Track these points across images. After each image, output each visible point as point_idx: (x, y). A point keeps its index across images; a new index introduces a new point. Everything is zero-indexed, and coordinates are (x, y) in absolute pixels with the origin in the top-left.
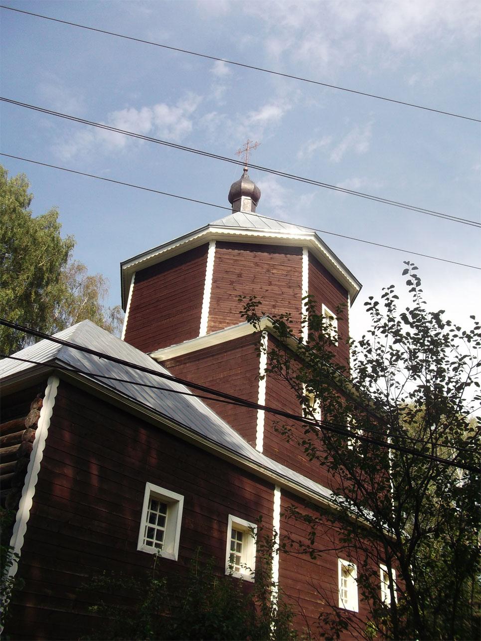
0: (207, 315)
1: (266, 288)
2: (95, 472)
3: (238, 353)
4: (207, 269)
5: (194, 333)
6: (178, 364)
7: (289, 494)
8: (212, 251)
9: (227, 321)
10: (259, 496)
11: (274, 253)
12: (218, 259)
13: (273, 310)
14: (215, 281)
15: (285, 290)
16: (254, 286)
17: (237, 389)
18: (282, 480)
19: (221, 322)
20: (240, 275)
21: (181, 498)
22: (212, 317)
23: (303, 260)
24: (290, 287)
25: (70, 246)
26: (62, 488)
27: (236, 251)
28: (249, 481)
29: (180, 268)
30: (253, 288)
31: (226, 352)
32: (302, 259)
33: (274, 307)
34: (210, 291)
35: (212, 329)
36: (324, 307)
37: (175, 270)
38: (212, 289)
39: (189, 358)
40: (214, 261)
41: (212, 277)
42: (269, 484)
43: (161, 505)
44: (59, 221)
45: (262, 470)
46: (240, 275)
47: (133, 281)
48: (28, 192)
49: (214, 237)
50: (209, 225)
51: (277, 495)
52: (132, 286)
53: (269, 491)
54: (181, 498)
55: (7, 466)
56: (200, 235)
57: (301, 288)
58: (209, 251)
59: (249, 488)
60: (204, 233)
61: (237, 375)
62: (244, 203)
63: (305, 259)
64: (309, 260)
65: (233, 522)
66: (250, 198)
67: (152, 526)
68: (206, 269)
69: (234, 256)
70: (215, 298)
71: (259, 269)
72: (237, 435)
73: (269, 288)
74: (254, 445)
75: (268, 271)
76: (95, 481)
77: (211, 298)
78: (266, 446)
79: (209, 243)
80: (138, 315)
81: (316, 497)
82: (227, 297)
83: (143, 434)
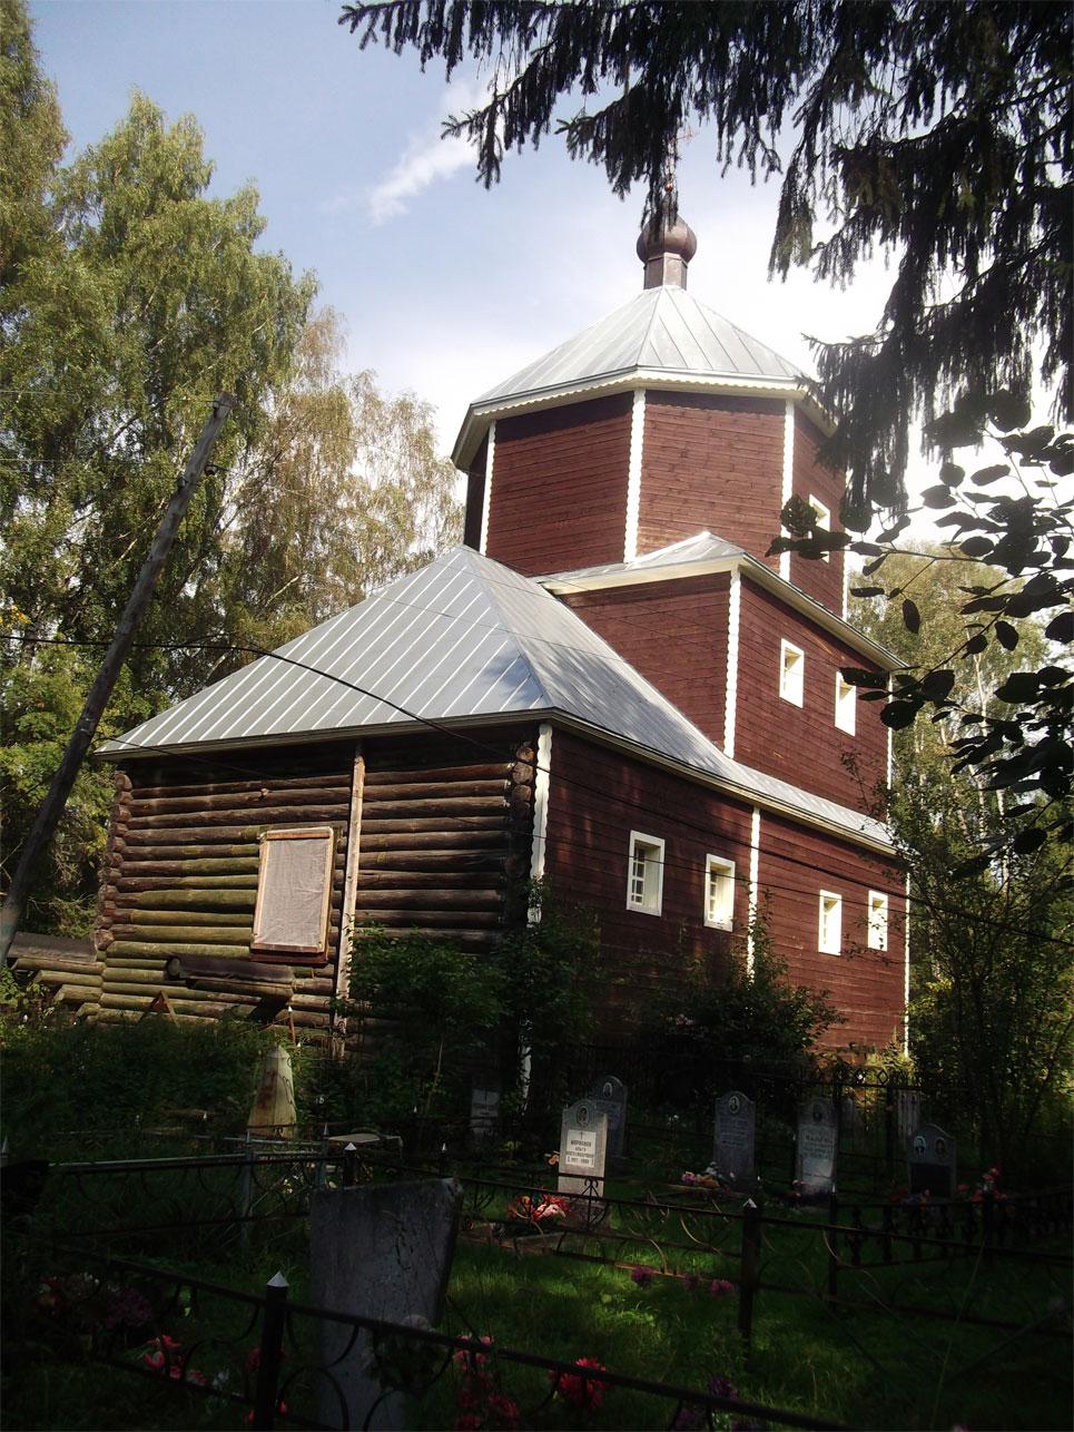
0: (636, 525)
1: (726, 475)
2: (589, 829)
3: (692, 601)
4: (632, 442)
5: (614, 554)
6: (591, 603)
7: (772, 816)
8: (639, 408)
9: (666, 536)
10: (737, 825)
11: (739, 411)
12: (652, 426)
13: (737, 516)
14: (646, 464)
15: (756, 479)
16: (708, 473)
17: (693, 659)
18: (764, 801)
19: (656, 538)
20: (684, 454)
21: (661, 843)
22: (643, 530)
23: (786, 425)
24: (763, 475)
25: (307, 294)
26: (564, 851)
27: (679, 409)
28: (726, 807)
29: (582, 428)
30: (707, 477)
31: (672, 596)
32: (784, 422)
33: (739, 509)
34: (639, 483)
35: (644, 549)
36: (812, 497)
37: (571, 431)
38: (643, 478)
39: (609, 597)
40: (645, 428)
41: (641, 458)
42: (746, 806)
43: (644, 851)
44: (261, 211)
45: (743, 793)
46: (684, 454)
47: (492, 437)
48: (205, 158)
49: (642, 385)
50: (637, 365)
51: (756, 817)
52: (491, 446)
53: (748, 815)
54: (661, 843)
55: (488, 822)
56: (621, 380)
57: (781, 475)
58: (634, 408)
59: (727, 815)
60: (629, 377)
61: (691, 636)
62: (668, 267)
63: (790, 421)
64: (795, 423)
65: (712, 863)
66: (678, 256)
67: (640, 879)
68: (629, 441)
69: (675, 417)
70: (648, 497)
71: (714, 441)
72: (695, 729)
73: (732, 476)
74: (721, 747)
75: (730, 446)
76: (589, 839)
77: (642, 495)
78: (738, 748)
79: (633, 392)
80: (508, 503)
81: (801, 815)
82: (664, 494)
83: (627, 774)
